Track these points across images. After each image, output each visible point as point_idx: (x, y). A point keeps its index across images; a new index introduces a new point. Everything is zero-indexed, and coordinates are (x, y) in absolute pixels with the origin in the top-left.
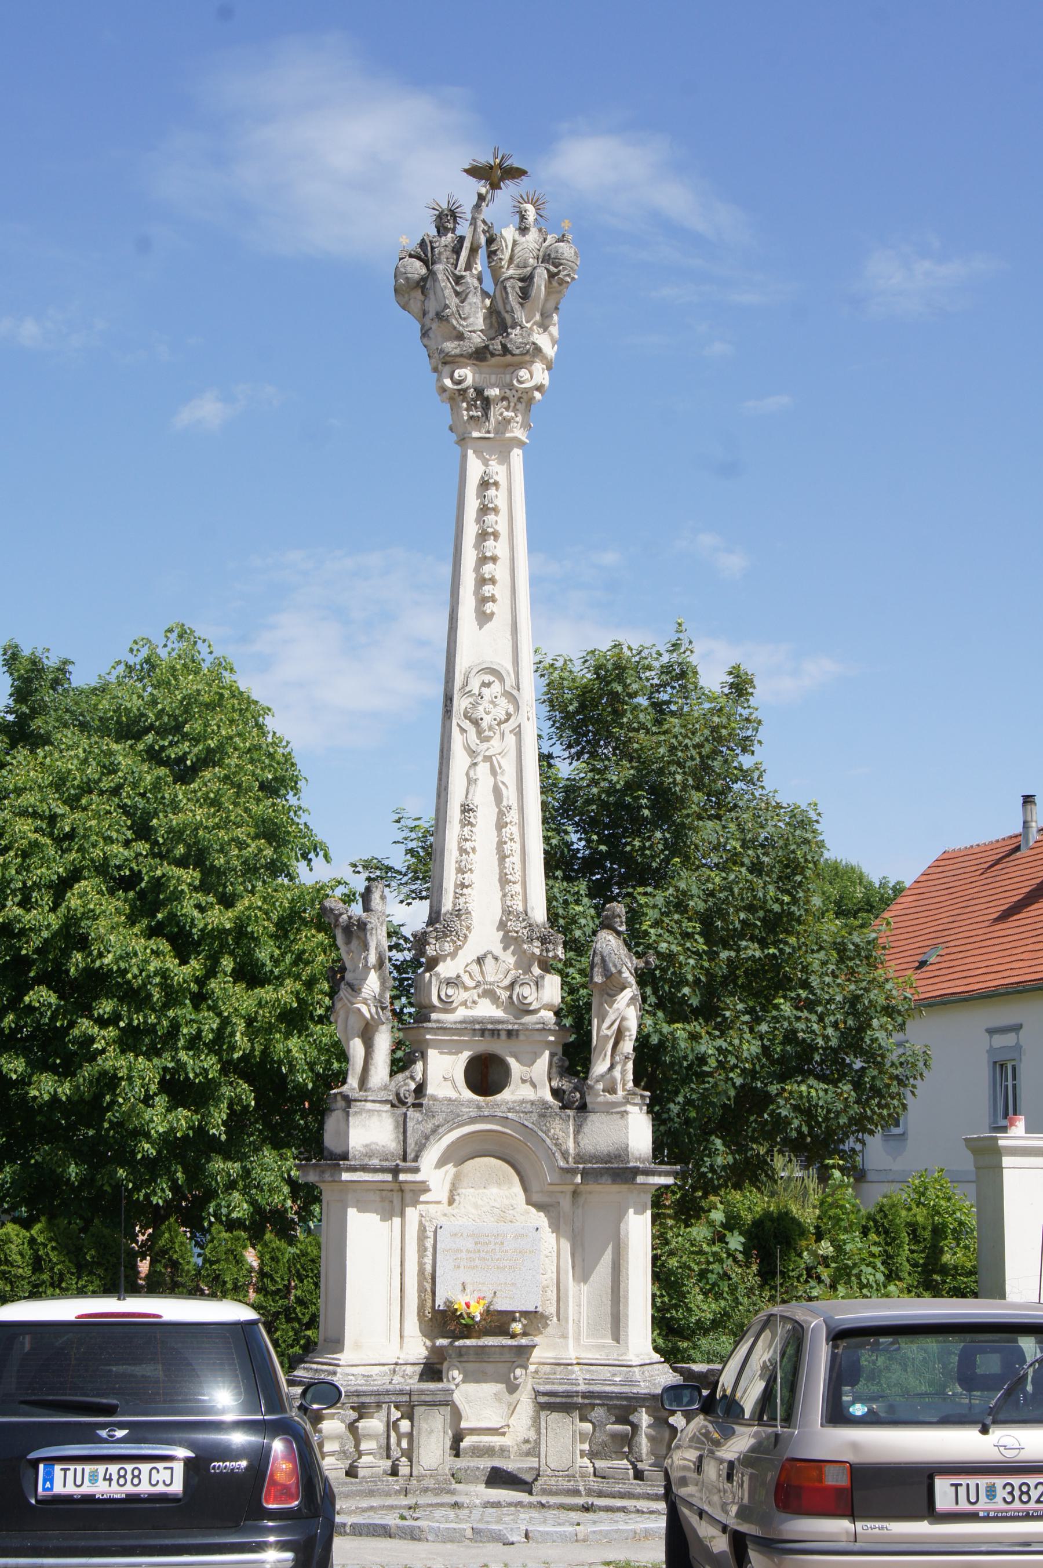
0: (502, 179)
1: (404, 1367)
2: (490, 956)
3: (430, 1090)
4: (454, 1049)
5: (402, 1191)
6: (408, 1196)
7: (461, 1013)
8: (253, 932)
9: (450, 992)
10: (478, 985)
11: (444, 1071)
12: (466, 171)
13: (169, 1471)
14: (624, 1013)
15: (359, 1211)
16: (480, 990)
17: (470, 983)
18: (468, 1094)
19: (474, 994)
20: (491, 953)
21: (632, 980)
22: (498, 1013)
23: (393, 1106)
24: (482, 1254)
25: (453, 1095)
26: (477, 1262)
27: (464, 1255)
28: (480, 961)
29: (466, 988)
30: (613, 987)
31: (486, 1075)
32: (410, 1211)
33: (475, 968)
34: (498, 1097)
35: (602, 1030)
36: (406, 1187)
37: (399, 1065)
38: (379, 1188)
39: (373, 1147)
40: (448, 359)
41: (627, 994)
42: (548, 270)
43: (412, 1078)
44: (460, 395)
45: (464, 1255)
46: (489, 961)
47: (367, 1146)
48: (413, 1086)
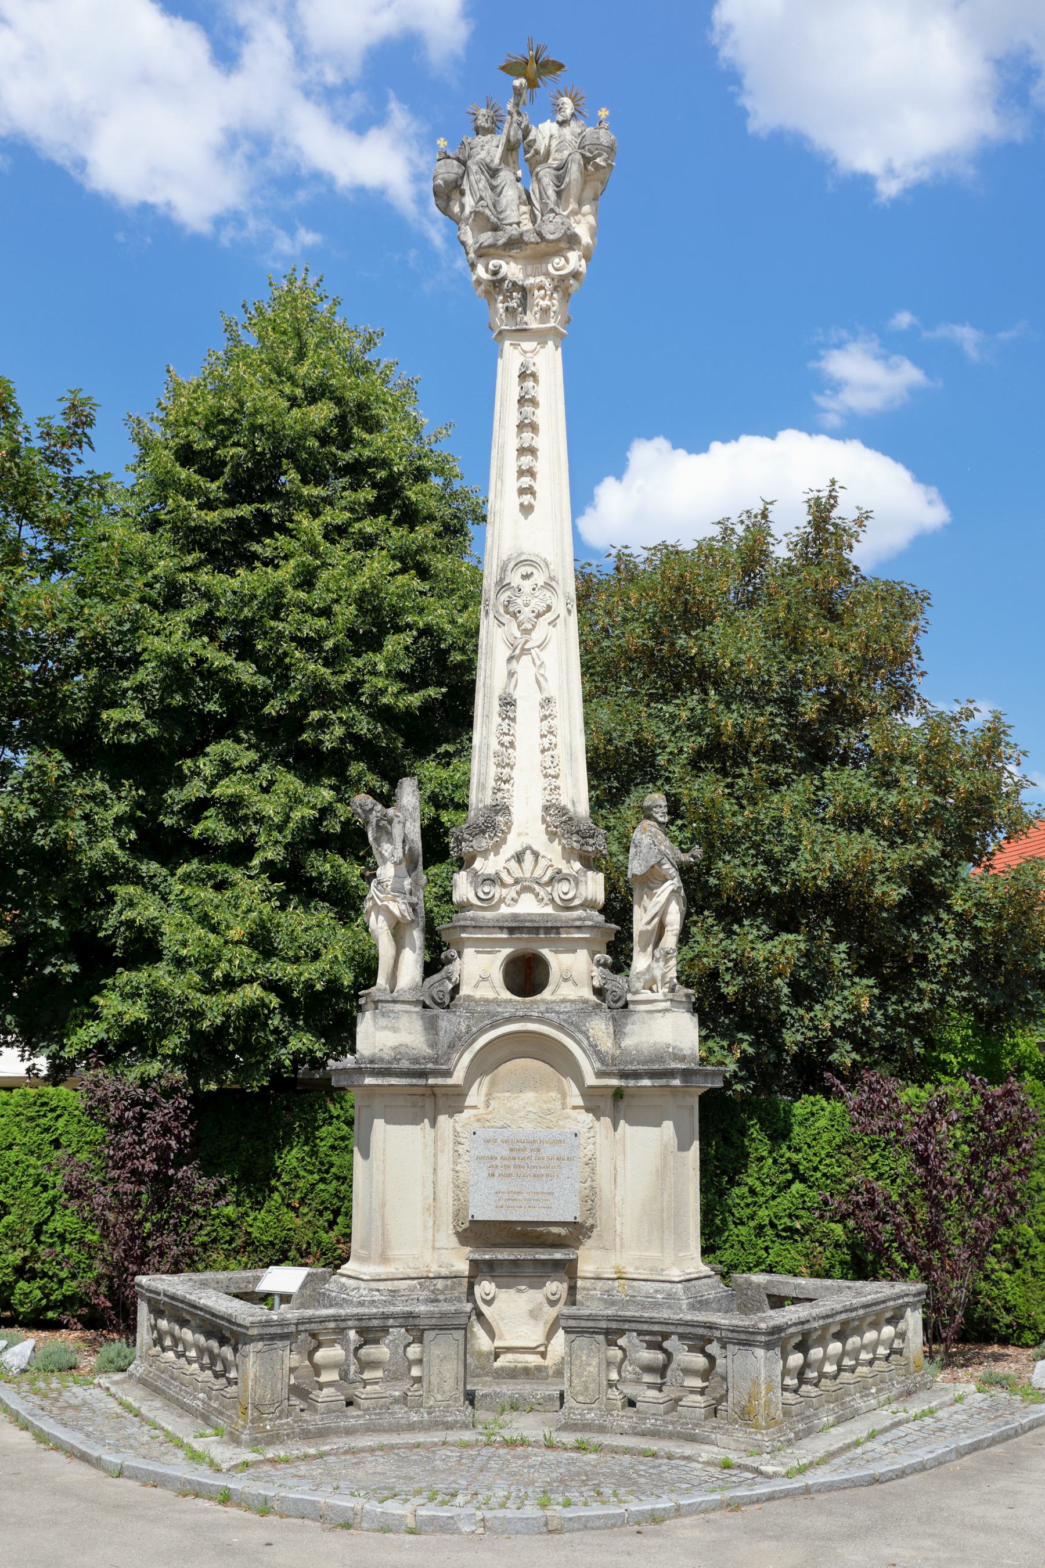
0: (539, 74)
1: (435, 1281)
2: (528, 852)
3: (464, 991)
4: (486, 946)
5: (434, 1095)
6: (441, 1102)
7: (504, 910)
8: (861, 831)
9: (486, 889)
10: (517, 881)
11: (480, 971)
12: (503, 68)
13: (437, 1245)
14: (660, 907)
15: (387, 1122)
16: (518, 887)
17: (509, 880)
18: (507, 995)
19: (512, 892)
20: (529, 848)
21: (673, 871)
22: (549, 910)
23: (425, 1006)
24: (517, 1162)
25: (490, 995)
26: (512, 1170)
27: (498, 1162)
28: (519, 857)
29: (503, 885)
30: (652, 879)
31: (526, 975)
32: (442, 1119)
33: (513, 865)
34: (538, 997)
35: (641, 920)
36: (437, 1091)
37: (431, 968)
38: (409, 1093)
39: (403, 1050)
40: (483, 251)
41: (668, 887)
42: (583, 156)
43: (449, 979)
44: (495, 287)
45: (498, 1162)
46: (528, 857)
47: (395, 1048)
48: (450, 986)
